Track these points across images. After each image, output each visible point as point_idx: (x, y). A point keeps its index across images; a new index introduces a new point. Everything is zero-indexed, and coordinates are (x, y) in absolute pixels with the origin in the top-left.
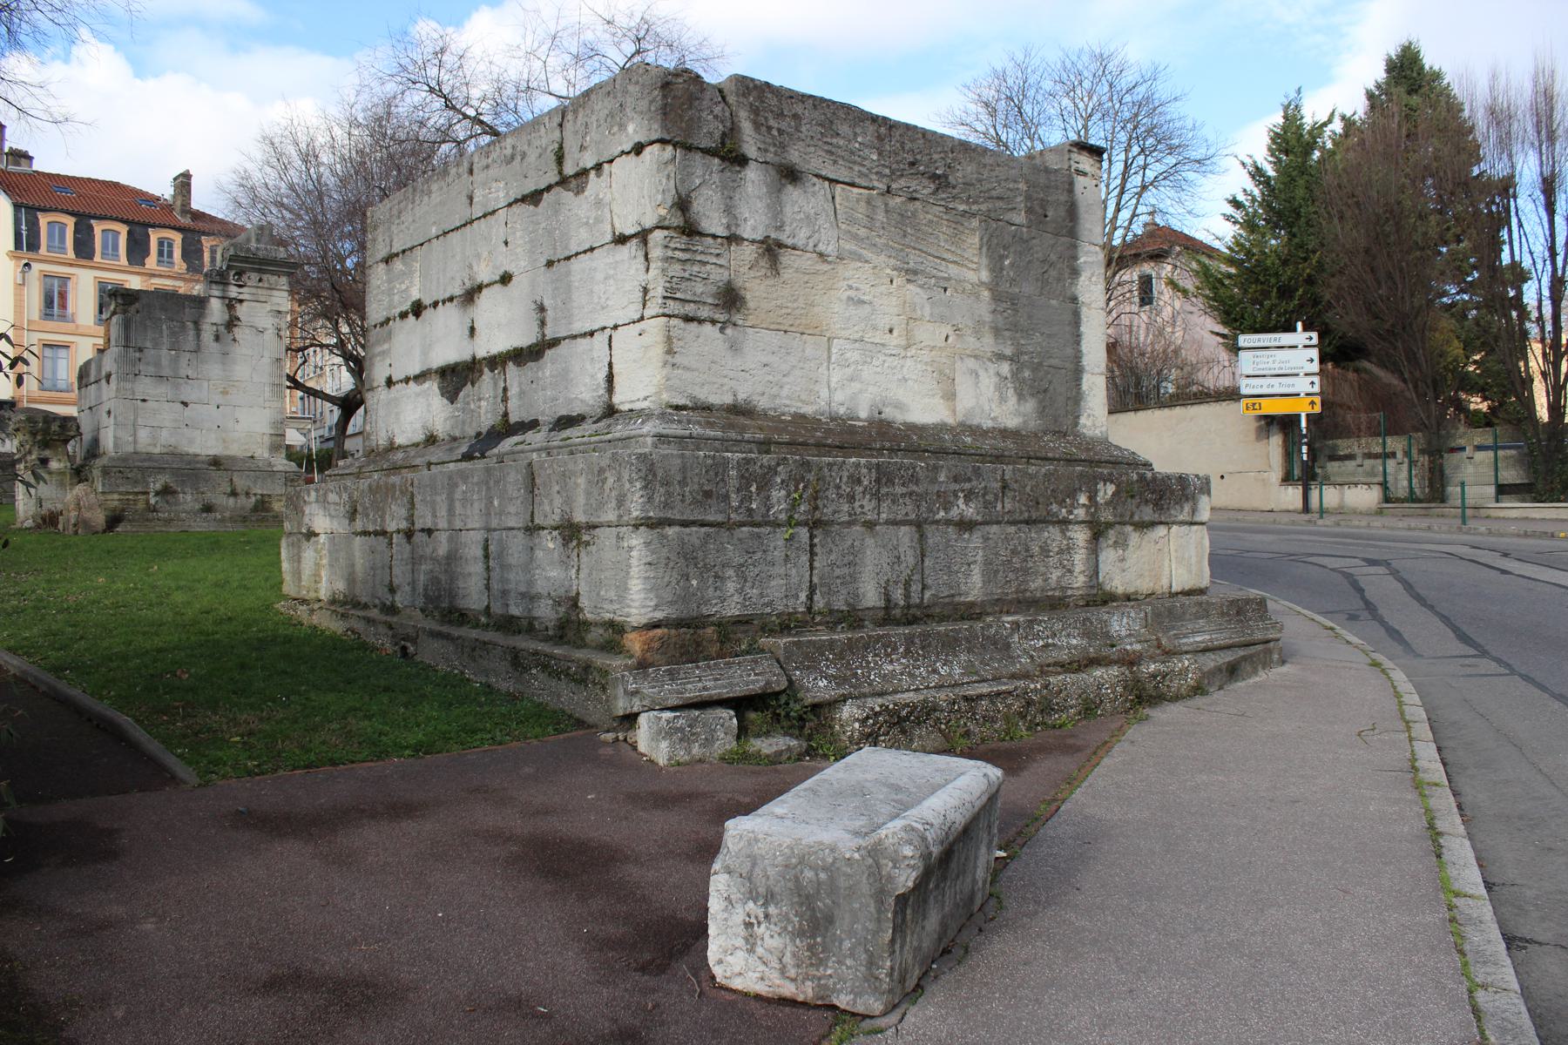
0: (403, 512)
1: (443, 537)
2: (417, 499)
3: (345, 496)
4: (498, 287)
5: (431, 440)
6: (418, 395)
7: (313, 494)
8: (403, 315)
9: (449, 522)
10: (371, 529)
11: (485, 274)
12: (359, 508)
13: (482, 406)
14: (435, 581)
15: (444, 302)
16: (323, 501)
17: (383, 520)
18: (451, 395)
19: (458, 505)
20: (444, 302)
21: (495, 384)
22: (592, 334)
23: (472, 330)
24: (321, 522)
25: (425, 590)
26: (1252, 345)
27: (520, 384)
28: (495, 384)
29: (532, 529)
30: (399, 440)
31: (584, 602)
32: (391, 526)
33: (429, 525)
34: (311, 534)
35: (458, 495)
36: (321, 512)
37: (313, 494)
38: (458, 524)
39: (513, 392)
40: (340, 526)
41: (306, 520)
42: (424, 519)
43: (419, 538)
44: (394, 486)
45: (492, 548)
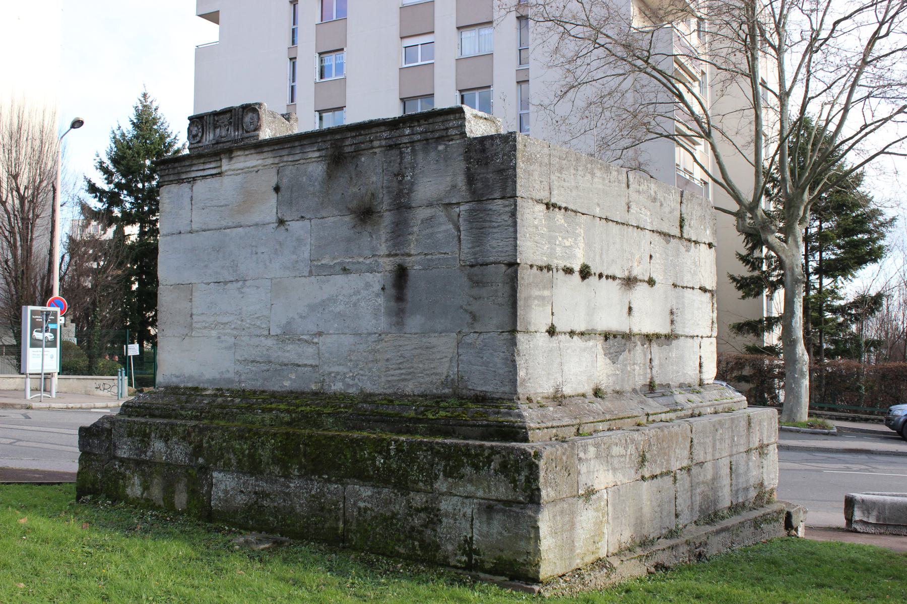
0: (686, 453)
1: (709, 466)
2: (695, 441)
3: (632, 449)
4: (646, 285)
5: (597, 393)
6: (584, 350)
7: (592, 450)
8: (569, 271)
9: (713, 455)
10: (658, 472)
11: (637, 272)
12: (648, 456)
13: (637, 367)
14: (705, 497)
15: (607, 277)
16: (605, 456)
17: (668, 461)
18: (613, 357)
19: (718, 442)
20: (607, 277)
21: (645, 355)
22: (692, 337)
23: (630, 309)
24: (601, 477)
25: (700, 506)
26: (46, 239)
27: (660, 358)
28: (645, 355)
29: (748, 451)
30: (567, 390)
31: (766, 483)
32: (675, 466)
33: (702, 460)
34: (590, 493)
35: (718, 437)
36: (602, 468)
37: (592, 450)
38: (717, 456)
39: (656, 363)
40: (627, 477)
41: (583, 479)
42: (699, 456)
43: (695, 470)
44: (677, 434)
45: (733, 467)
